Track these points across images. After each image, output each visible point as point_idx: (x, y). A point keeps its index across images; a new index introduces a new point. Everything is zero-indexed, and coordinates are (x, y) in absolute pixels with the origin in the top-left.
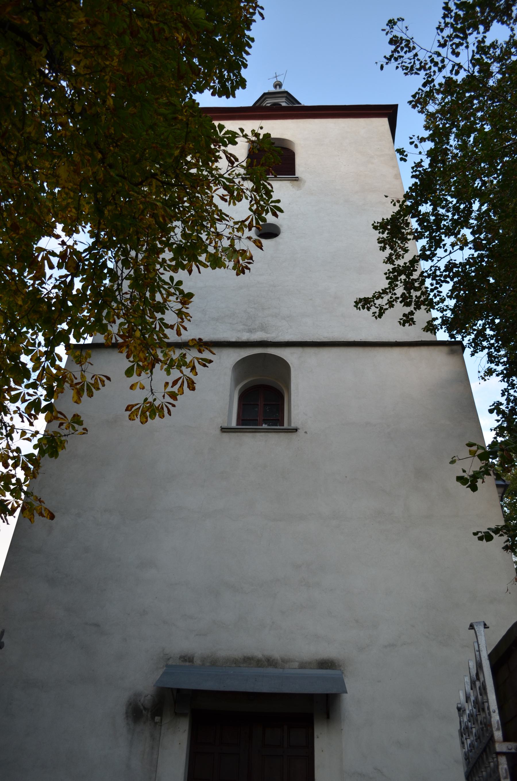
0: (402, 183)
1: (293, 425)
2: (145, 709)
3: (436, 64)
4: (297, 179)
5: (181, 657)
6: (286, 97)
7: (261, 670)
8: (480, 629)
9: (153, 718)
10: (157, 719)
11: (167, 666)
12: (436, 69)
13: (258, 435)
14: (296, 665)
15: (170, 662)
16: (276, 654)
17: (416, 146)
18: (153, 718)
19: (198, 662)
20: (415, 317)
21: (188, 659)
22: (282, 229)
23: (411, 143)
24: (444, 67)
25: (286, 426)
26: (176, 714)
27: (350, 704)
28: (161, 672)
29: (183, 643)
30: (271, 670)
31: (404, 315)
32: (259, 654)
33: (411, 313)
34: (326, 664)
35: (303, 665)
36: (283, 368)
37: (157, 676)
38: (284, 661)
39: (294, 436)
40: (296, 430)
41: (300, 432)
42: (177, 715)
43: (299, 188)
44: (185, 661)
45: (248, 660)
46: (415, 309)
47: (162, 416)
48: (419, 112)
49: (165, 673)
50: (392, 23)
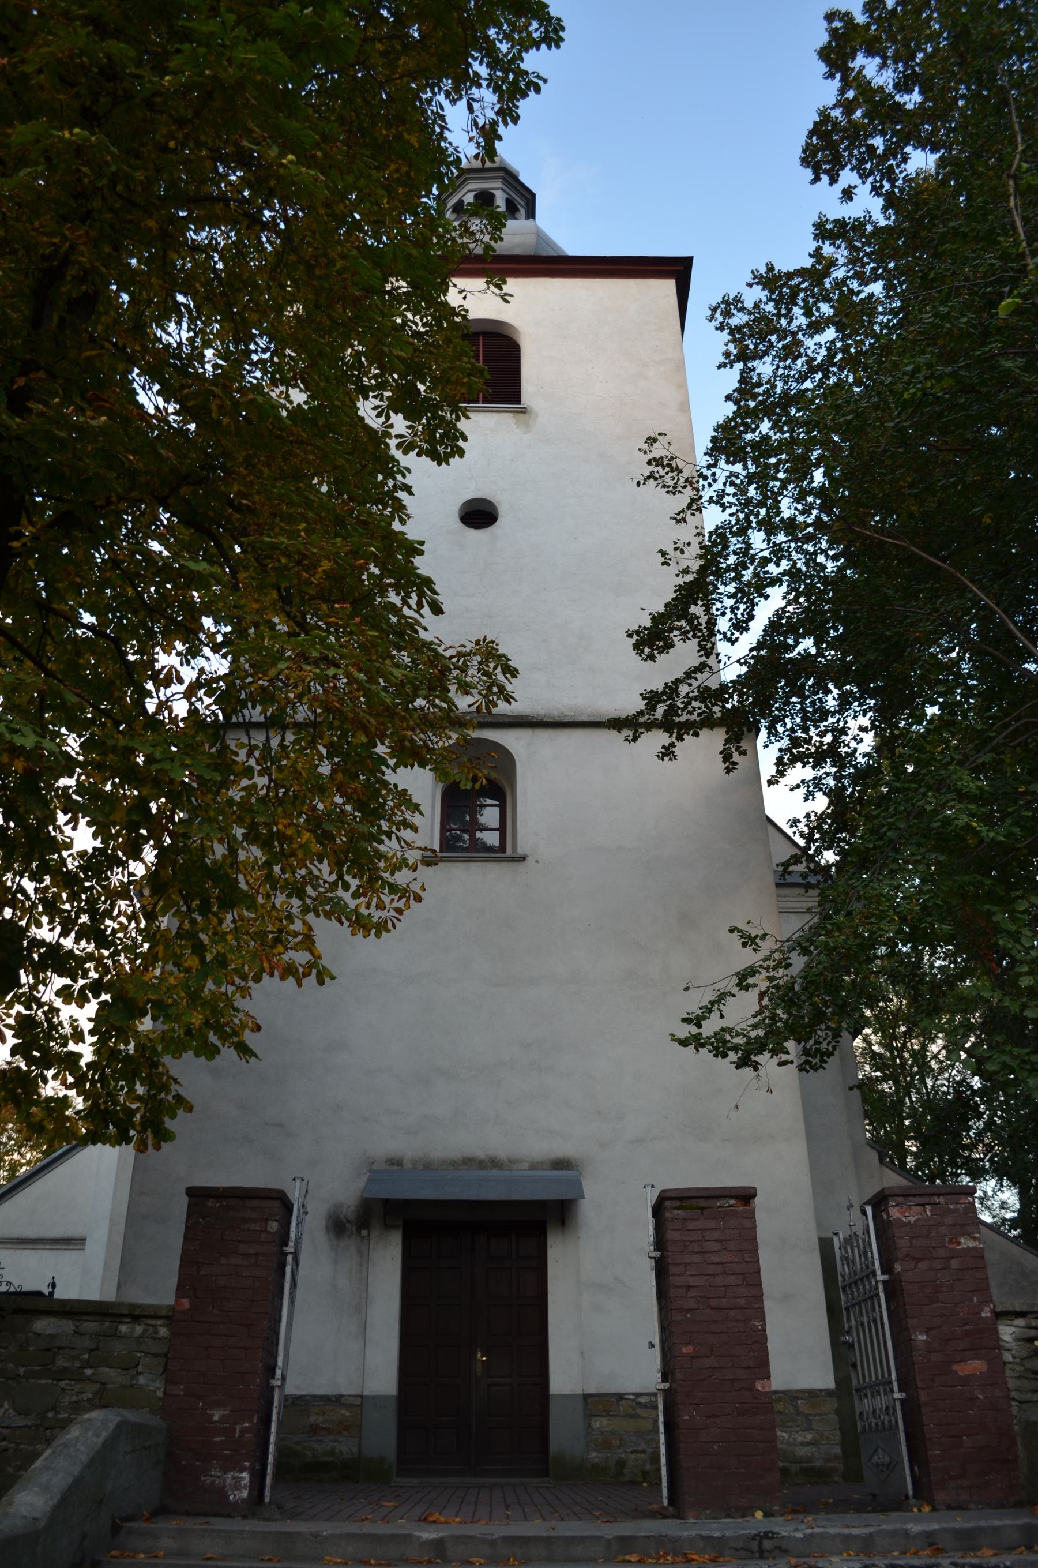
0: (119, 1287)
1: (520, 851)
2: (348, 1221)
3: (705, 478)
4: (524, 411)
5: (387, 1161)
6: (503, 178)
7: (485, 1173)
8: (649, 1189)
9: (359, 1232)
10: (364, 1232)
11: (371, 1171)
12: (706, 483)
13: (473, 865)
14: (526, 1165)
15: (375, 1167)
16: (502, 1154)
17: (682, 552)
18: (359, 1232)
19: (408, 1165)
20: (677, 751)
21: (396, 1162)
22: (502, 511)
23: (676, 549)
24: (715, 481)
25: (509, 852)
26: (386, 1225)
27: (587, 1210)
28: (365, 1178)
29: (390, 1144)
30: (495, 1173)
31: (664, 747)
32: (481, 1154)
33: (672, 745)
34: (562, 1164)
35: (533, 1166)
36: (506, 760)
37: (361, 1183)
38: (510, 1161)
39: (520, 867)
40: (523, 859)
41: (530, 861)
42: (387, 1226)
43: (527, 427)
44: (393, 1164)
45: (468, 1162)
46: (677, 739)
47: (388, 931)
48: (717, 328)
49: (370, 1181)
50: (652, 440)
